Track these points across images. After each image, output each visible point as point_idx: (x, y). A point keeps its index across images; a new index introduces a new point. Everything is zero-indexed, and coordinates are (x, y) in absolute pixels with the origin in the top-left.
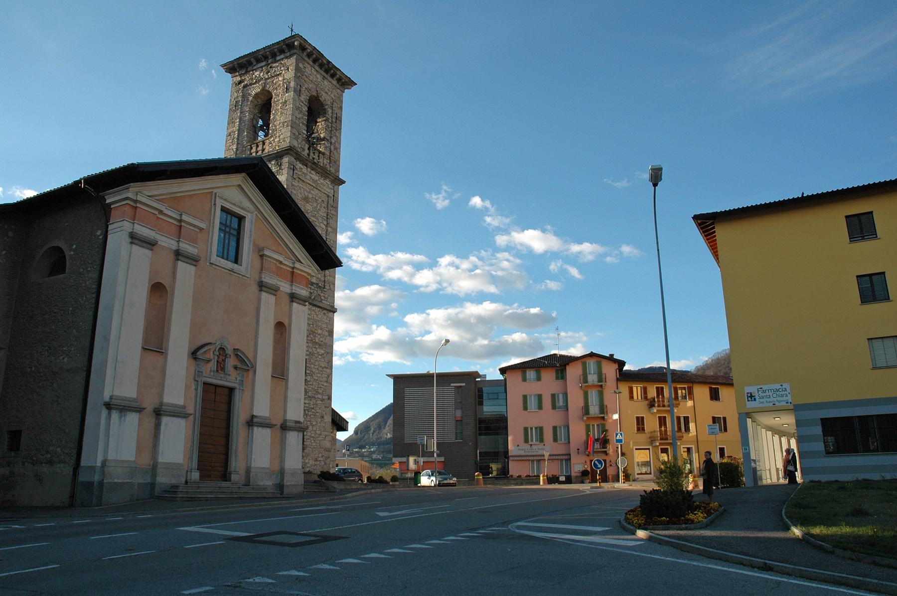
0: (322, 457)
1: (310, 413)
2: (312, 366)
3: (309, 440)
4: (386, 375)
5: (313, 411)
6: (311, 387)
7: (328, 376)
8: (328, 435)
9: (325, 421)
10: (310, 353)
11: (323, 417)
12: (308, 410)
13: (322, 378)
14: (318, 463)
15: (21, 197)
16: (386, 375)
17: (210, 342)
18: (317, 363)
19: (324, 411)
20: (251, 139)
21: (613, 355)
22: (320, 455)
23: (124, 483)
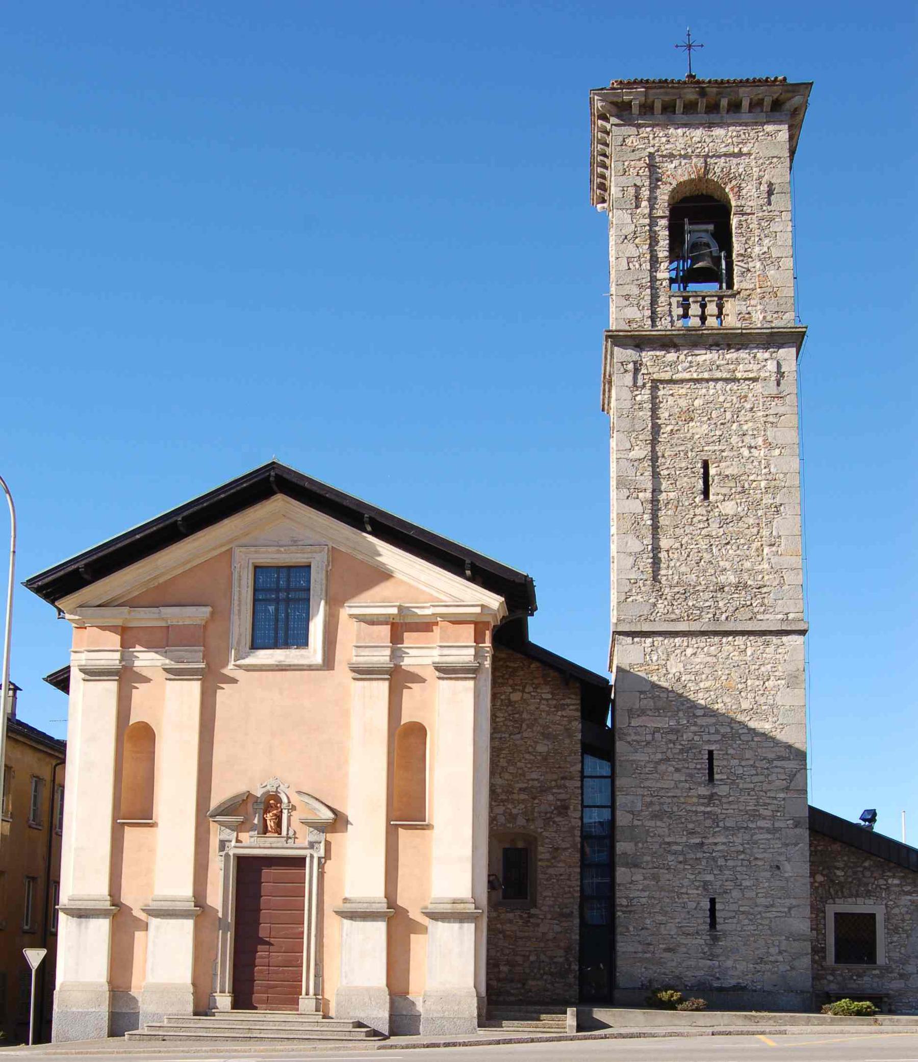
0: (780, 953)
1: (730, 863)
2: (734, 762)
3: (735, 921)
4: (335, 912)
5: (742, 857)
6: (736, 807)
7: (792, 776)
8: (794, 907)
9: (786, 875)
10: (723, 736)
11: (778, 867)
12: (724, 857)
13: (770, 783)
14: (769, 967)
15: (614, 1015)
16: (335, 912)
17: (347, 923)
18: (748, 754)
19: (780, 854)
20: (391, 620)
21: (870, 816)
22: (773, 950)
23: (87, 1014)
